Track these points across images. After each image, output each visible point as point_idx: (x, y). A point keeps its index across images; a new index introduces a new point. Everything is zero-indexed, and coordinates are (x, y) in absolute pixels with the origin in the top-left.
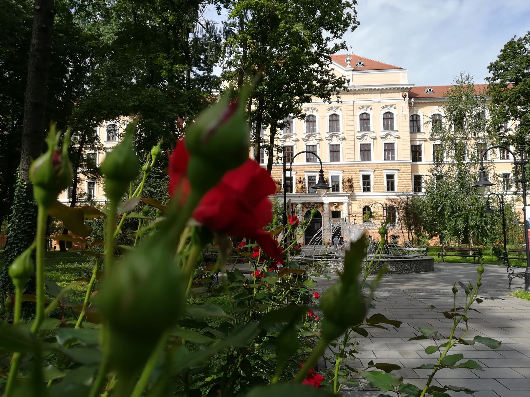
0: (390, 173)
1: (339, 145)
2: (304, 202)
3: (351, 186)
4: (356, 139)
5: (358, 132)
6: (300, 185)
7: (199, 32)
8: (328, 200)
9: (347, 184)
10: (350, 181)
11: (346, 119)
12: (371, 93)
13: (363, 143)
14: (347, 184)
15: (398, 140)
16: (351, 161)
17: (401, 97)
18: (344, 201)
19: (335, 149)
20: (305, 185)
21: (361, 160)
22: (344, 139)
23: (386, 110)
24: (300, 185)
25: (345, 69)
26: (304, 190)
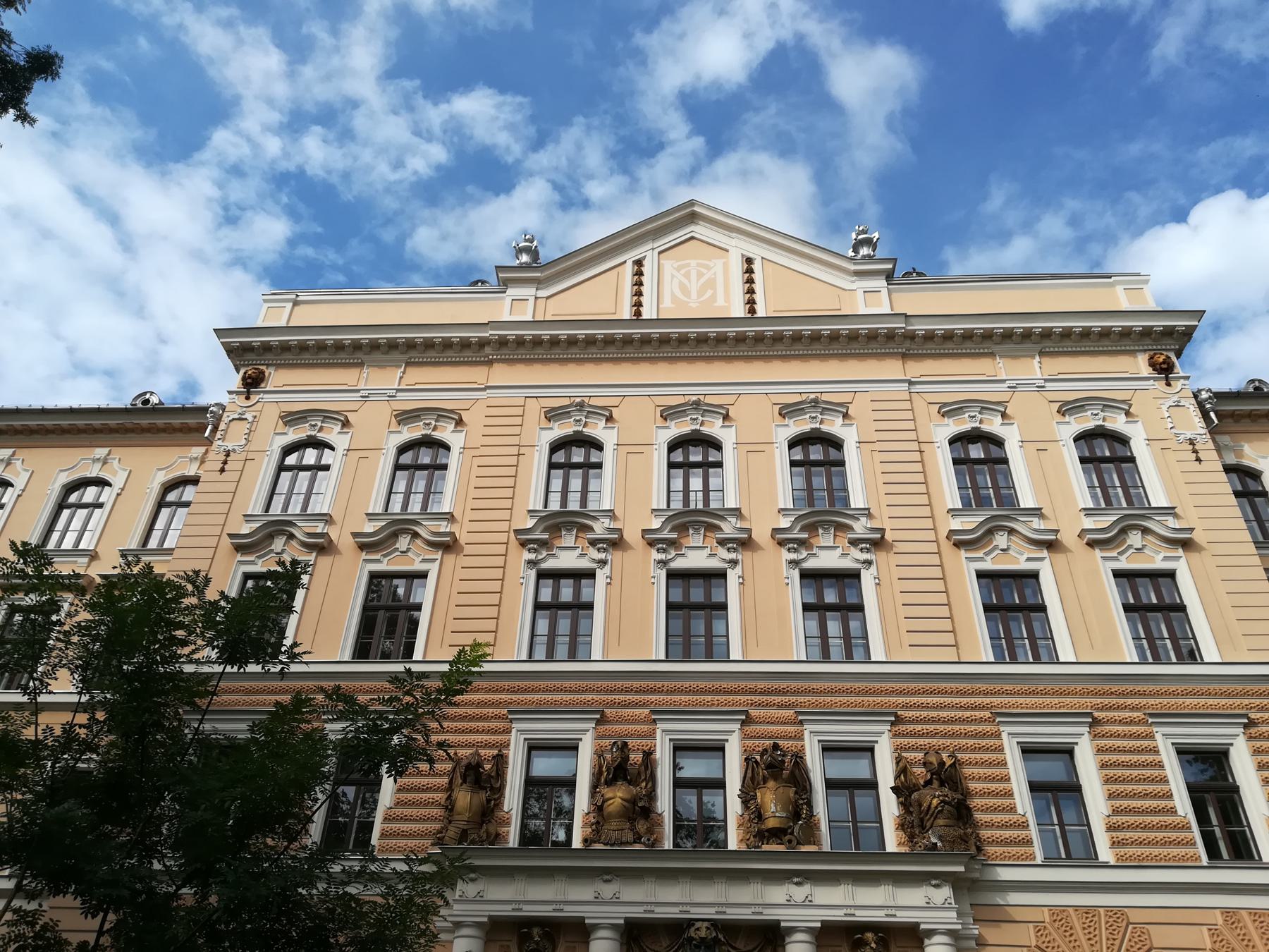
0: (1203, 735)
1: (722, 575)
2: (637, 912)
3: (961, 812)
4: (946, 547)
5: (953, 512)
6: (617, 796)
7: (1156, 71)
8: (808, 903)
9: (933, 798)
10: (947, 776)
11: (879, 457)
12: (992, 355)
13: (988, 565)
14: (933, 798)
15: (450, 559)
16: (936, 660)
17: (1146, 371)
18: (926, 919)
19: (697, 595)
20: (651, 795)
21: (999, 660)
22: (878, 543)
23: (964, 424)
24: (617, 796)
25: (853, 267)
26: (641, 826)
